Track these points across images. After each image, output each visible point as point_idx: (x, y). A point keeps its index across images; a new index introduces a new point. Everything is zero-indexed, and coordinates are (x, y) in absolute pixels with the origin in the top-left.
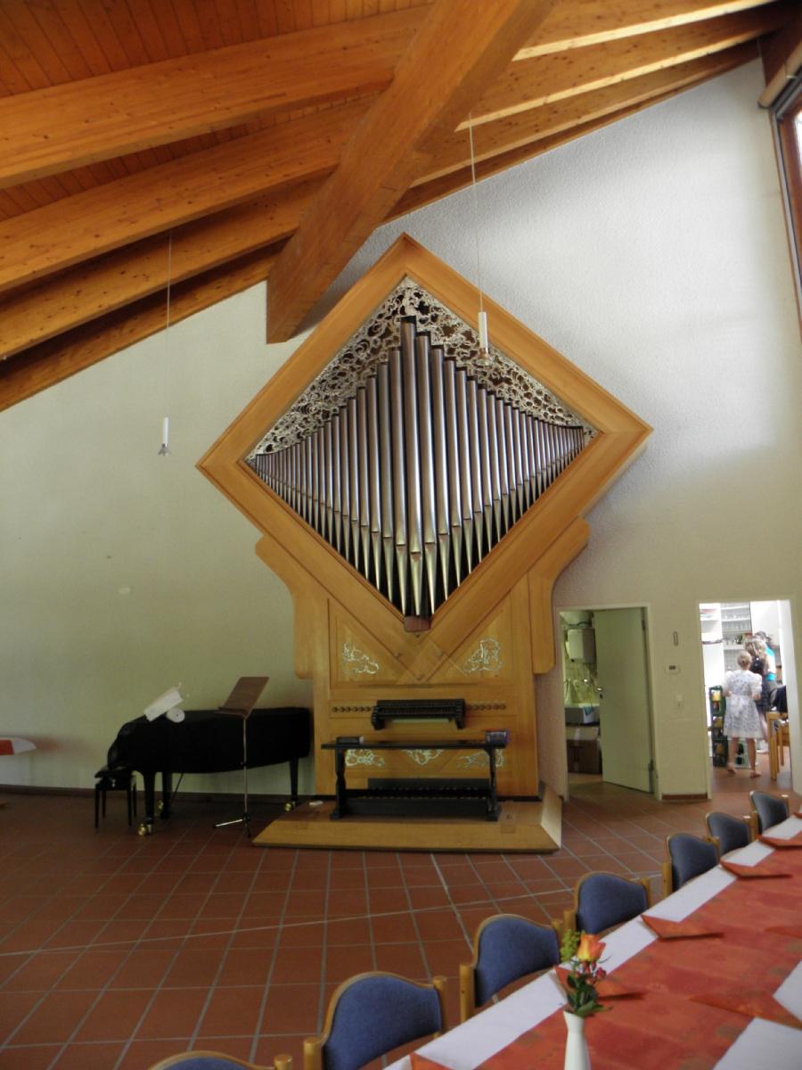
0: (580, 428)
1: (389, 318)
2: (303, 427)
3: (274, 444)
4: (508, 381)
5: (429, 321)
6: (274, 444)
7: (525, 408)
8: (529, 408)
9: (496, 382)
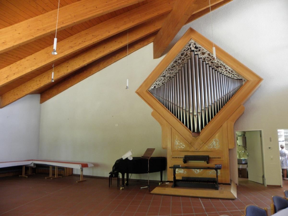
3: (156, 86)
4: (221, 67)
5: (198, 51)
6: (156, 86)
8: (227, 74)
9: (217, 67)
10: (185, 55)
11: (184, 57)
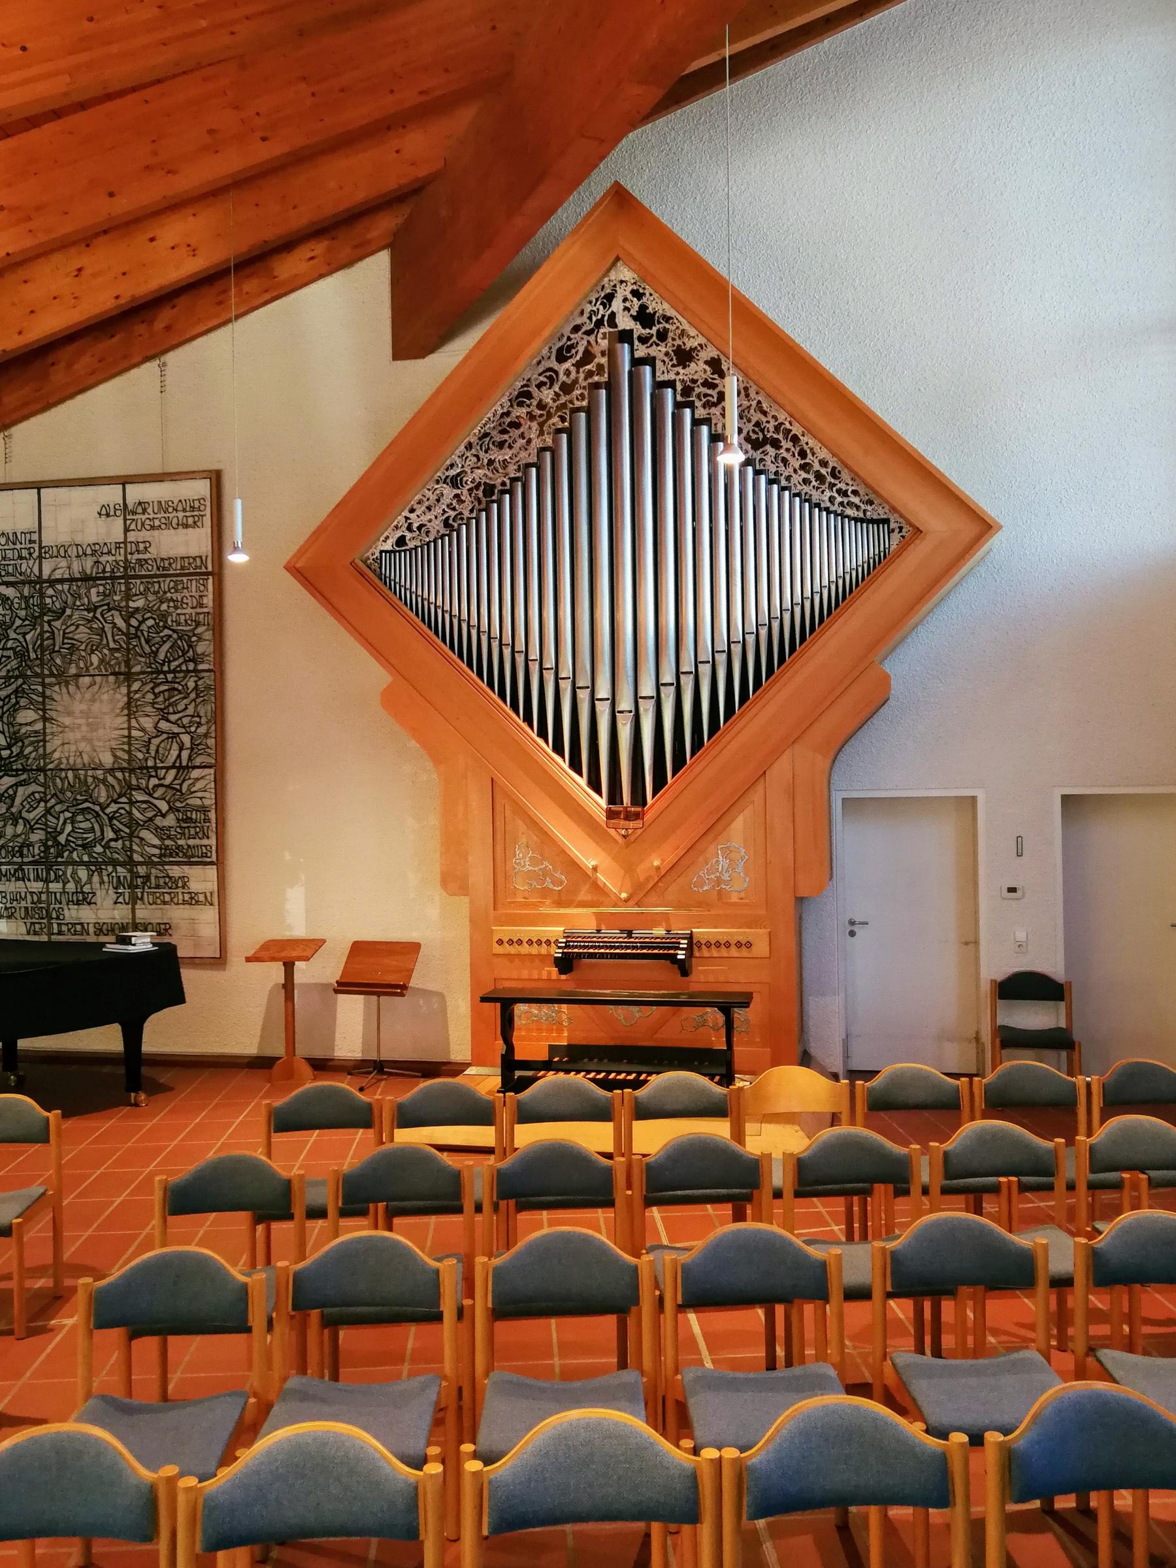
0: (886, 521)
1: (589, 333)
2: (454, 509)
3: (408, 535)
4: (776, 444)
5: (654, 339)
6: (408, 535)
7: (799, 487)
8: (806, 489)
10: (578, 358)
11: (573, 369)
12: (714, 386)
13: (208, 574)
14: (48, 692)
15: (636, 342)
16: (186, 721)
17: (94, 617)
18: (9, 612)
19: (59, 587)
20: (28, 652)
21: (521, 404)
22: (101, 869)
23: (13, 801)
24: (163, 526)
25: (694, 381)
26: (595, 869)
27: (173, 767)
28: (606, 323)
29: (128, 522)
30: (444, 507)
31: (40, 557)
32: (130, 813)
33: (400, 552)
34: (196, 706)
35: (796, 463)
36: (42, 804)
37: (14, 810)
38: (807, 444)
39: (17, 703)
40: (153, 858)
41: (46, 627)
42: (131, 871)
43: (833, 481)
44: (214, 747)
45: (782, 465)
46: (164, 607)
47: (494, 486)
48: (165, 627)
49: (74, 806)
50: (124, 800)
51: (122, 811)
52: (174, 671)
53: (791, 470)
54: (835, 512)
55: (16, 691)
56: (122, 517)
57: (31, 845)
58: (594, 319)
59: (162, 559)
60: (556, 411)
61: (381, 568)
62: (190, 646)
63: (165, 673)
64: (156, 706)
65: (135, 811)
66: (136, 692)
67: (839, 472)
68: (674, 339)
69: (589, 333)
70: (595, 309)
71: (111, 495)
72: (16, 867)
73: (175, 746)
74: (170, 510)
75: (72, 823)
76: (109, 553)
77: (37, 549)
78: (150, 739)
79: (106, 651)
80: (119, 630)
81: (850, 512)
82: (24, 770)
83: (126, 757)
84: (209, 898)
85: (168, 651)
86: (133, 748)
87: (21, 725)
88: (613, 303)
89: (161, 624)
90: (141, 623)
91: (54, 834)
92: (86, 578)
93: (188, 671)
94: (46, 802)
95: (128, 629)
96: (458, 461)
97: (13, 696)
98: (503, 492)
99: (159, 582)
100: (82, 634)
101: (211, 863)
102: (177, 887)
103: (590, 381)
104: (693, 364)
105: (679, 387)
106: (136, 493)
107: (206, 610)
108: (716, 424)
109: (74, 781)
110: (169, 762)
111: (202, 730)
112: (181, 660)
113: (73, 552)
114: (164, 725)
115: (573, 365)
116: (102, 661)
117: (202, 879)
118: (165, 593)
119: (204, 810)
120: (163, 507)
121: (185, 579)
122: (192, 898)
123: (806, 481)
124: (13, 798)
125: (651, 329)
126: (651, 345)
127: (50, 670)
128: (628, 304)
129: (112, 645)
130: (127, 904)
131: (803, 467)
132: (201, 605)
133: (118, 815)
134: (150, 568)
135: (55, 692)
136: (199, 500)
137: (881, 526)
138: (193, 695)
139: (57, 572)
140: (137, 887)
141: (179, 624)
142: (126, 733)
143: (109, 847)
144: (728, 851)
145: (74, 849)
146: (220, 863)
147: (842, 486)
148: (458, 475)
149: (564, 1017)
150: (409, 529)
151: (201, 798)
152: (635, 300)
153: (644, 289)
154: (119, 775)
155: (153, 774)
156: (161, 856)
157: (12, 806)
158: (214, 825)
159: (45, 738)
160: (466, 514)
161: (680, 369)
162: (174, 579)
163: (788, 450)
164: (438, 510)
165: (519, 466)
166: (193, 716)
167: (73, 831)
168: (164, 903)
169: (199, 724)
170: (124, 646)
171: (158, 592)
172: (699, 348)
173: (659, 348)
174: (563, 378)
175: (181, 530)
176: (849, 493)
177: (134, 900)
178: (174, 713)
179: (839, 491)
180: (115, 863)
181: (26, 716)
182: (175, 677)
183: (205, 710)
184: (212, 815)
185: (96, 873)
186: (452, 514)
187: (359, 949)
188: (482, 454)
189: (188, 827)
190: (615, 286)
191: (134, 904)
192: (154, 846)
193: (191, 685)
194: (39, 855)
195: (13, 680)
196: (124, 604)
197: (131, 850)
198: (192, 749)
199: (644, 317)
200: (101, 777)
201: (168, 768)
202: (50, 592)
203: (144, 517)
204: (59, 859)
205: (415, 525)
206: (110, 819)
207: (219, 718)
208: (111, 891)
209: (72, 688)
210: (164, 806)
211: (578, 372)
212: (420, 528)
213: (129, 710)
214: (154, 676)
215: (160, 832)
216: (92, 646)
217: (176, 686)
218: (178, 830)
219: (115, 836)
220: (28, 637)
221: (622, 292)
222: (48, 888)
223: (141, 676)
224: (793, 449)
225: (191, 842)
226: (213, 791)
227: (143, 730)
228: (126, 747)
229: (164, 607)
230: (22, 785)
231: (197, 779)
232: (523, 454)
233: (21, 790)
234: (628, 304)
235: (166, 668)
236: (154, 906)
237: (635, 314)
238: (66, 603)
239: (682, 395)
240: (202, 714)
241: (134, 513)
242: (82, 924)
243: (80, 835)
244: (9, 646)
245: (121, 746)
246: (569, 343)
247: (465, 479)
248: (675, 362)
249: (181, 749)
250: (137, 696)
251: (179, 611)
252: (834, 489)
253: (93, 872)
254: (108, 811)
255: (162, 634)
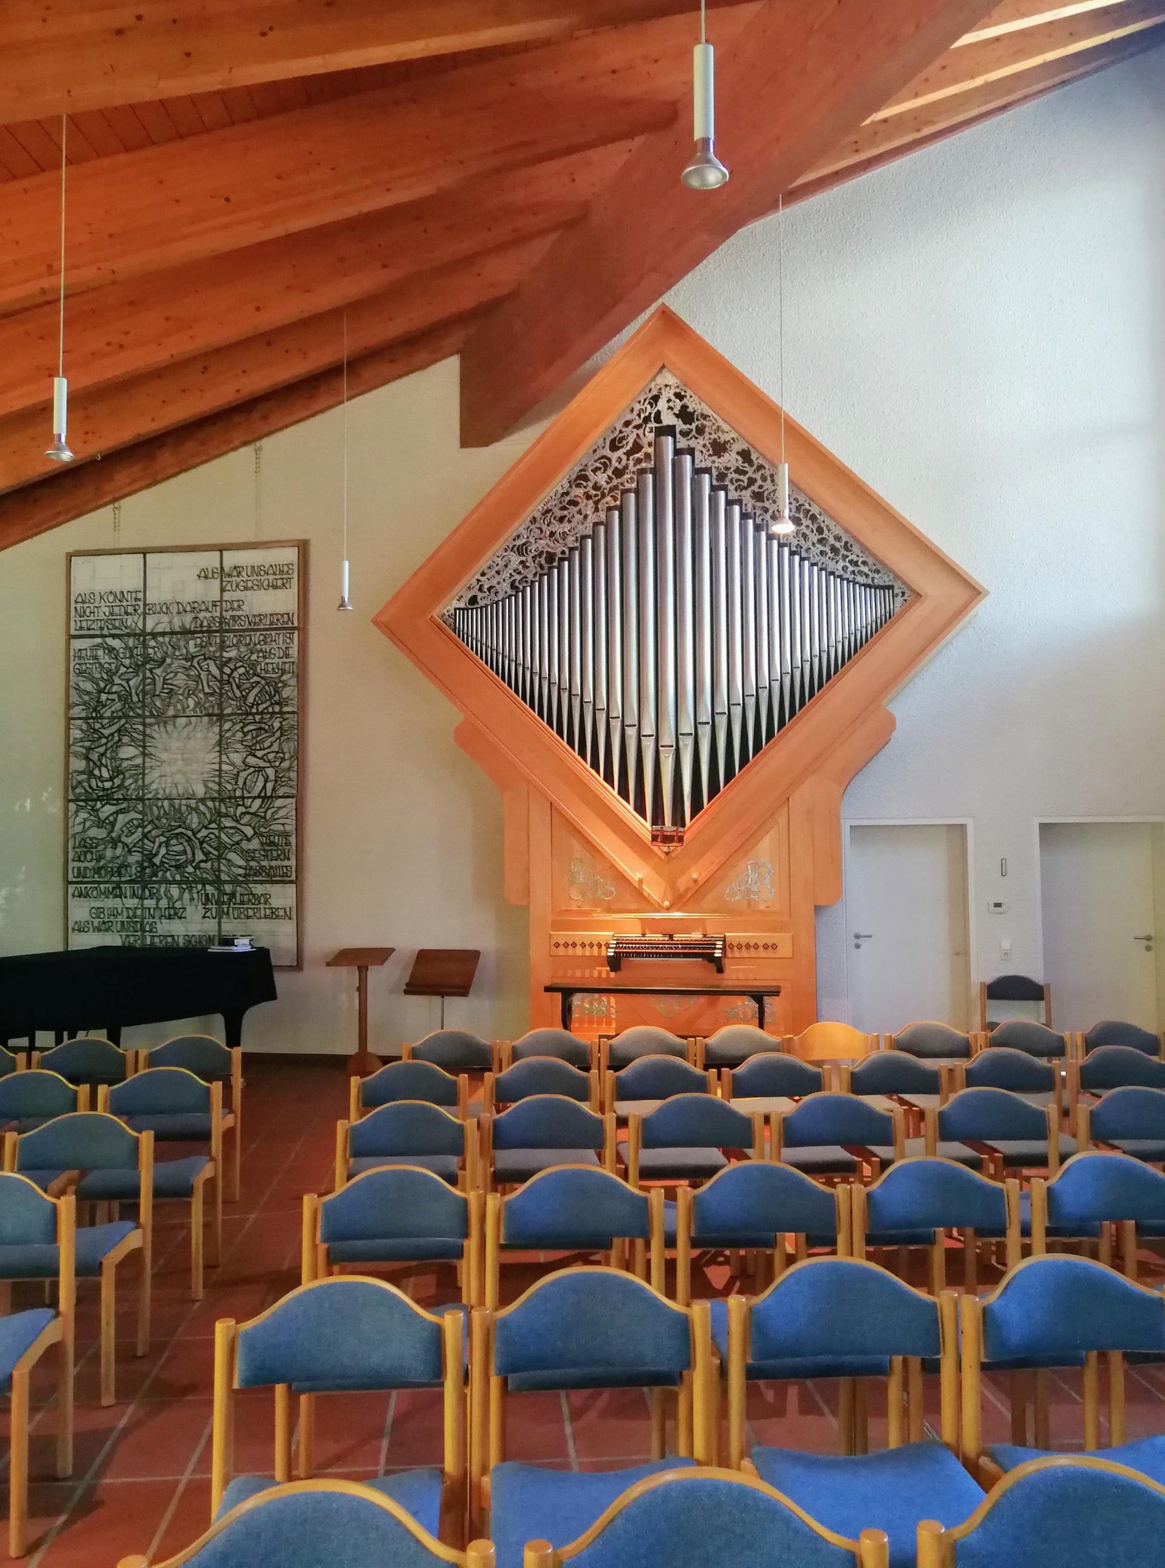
0: (891, 587)
2: (519, 573)
3: (480, 595)
5: (694, 433)
6: (480, 595)
7: (817, 558)
8: (823, 559)
11: (624, 458)
12: (745, 473)
13: (294, 628)
14: (148, 731)
15: (678, 436)
16: (271, 756)
17: (192, 665)
18: (114, 661)
19: (161, 639)
20: (131, 695)
21: (578, 486)
22: (191, 887)
23: (113, 826)
24: (255, 587)
25: (727, 469)
26: (641, 881)
27: (259, 797)
28: (652, 419)
29: (224, 584)
30: (512, 571)
31: (144, 614)
32: (219, 837)
33: (472, 609)
34: (280, 744)
35: (814, 538)
36: (140, 830)
37: (114, 835)
38: (824, 522)
39: (120, 740)
40: (239, 878)
41: (148, 674)
42: (218, 889)
43: (845, 553)
44: (295, 779)
45: (803, 539)
46: (254, 657)
47: (555, 554)
48: (255, 675)
49: (168, 831)
50: (213, 825)
51: (212, 836)
52: (262, 713)
53: (810, 544)
54: (847, 579)
55: (119, 731)
56: (219, 579)
57: (129, 866)
58: (643, 416)
59: (254, 616)
60: (609, 492)
61: (455, 623)
62: (276, 691)
63: (253, 714)
64: (244, 743)
65: (223, 836)
66: (227, 731)
67: (851, 546)
68: (710, 434)
69: (638, 427)
70: (643, 407)
71: (211, 560)
72: (114, 885)
73: (261, 779)
74: (262, 573)
75: (167, 847)
76: (207, 610)
77: (142, 606)
78: (238, 772)
79: (201, 695)
80: (213, 676)
81: (860, 579)
82: (125, 799)
83: (216, 788)
84: (288, 913)
85: (256, 695)
86: (223, 780)
87: (123, 759)
88: (658, 403)
89: (251, 672)
90: (233, 671)
91: (151, 856)
92: (185, 632)
93: (274, 713)
94: (144, 827)
95: (222, 677)
96: (524, 532)
97: (116, 735)
98: (562, 560)
99: (250, 635)
100: (180, 680)
101: (291, 882)
102: (260, 903)
103: (639, 467)
104: (726, 455)
105: (715, 473)
106: (232, 559)
107: (291, 660)
108: (746, 505)
109: (170, 809)
110: (255, 793)
111: (286, 764)
112: (268, 703)
113: (174, 609)
114: (251, 760)
115: (624, 454)
116: (197, 704)
117: (282, 896)
118: (255, 645)
119: (286, 835)
120: (256, 570)
121: (273, 633)
122: (273, 913)
123: (822, 553)
124: (113, 824)
125: (691, 424)
126: (691, 438)
127: (151, 712)
128: (671, 404)
129: (207, 690)
130: (215, 918)
131: (821, 541)
132: (287, 656)
133: (208, 839)
134: (243, 623)
135: (153, 731)
136: (288, 565)
137: (887, 591)
138: (278, 734)
139: (160, 626)
140: (224, 903)
141: (267, 672)
142: (217, 767)
143: (200, 868)
144: (756, 866)
145: (168, 870)
146: (298, 882)
147: (855, 558)
148: (524, 544)
149: (613, 1010)
150: (480, 589)
151: (283, 824)
152: (677, 400)
153: (685, 392)
154: (210, 804)
155: (241, 803)
156: (245, 875)
157: (112, 831)
158: (294, 848)
159: (144, 771)
160: (530, 577)
161: (715, 458)
162: (264, 633)
163: (807, 527)
164: (505, 575)
165: (577, 537)
166: (277, 752)
167: (167, 853)
168: (248, 917)
169: (283, 760)
170: (217, 690)
171: (249, 644)
172: (732, 442)
173: (698, 441)
174: (615, 464)
175: (271, 590)
176: (859, 563)
177: (220, 915)
178: (261, 749)
179: (851, 562)
180: (204, 882)
181: (127, 752)
182: (262, 718)
183: (289, 747)
184: (293, 840)
185: (187, 891)
186: (518, 577)
187: (424, 956)
188: (544, 527)
189: (270, 850)
190: (660, 389)
191: (221, 918)
192: (240, 867)
193: (277, 725)
194: (135, 874)
195: (116, 720)
196: (218, 654)
197: (219, 870)
198: (276, 781)
199: (685, 415)
200: (194, 806)
201: (254, 798)
202: (152, 643)
203: (238, 580)
204: (154, 879)
205: (486, 587)
206: (201, 843)
207: (300, 755)
208: (200, 907)
209: (170, 728)
210: (249, 831)
211: (628, 459)
212: (489, 589)
213: (220, 747)
214: (244, 717)
215: (247, 855)
216: (189, 690)
217: (263, 725)
218: (262, 853)
219: (204, 858)
220: (132, 683)
221: (667, 394)
222: (142, 904)
223: (232, 717)
224: (811, 526)
225: (274, 863)
226: (294, 818)
227: (232, 764)
228: (217, 779)
229: (254, 657)
230: (122, 813)
231: (280, 808)
232: (580, 527)
233: (121, 816)
234: (671, 404)
235: (254, 710)
236: (238, 920)
237: (677, 412)
238: (166, 653)
239: (717, 480)
240: (285, 750)
241: (230, 575)
242: (172, 936)
243: (173, 857)
244: (114, 690)
245: (212, 779)
246: (621, 435)
247: (529, 548)
248: (711, 452)
249: (266, 782)
250: (228, 735)
251: (267, 661)
252: (847, 560)
253: (184, 889)
254: (199, 835)
255: (252, 681)
